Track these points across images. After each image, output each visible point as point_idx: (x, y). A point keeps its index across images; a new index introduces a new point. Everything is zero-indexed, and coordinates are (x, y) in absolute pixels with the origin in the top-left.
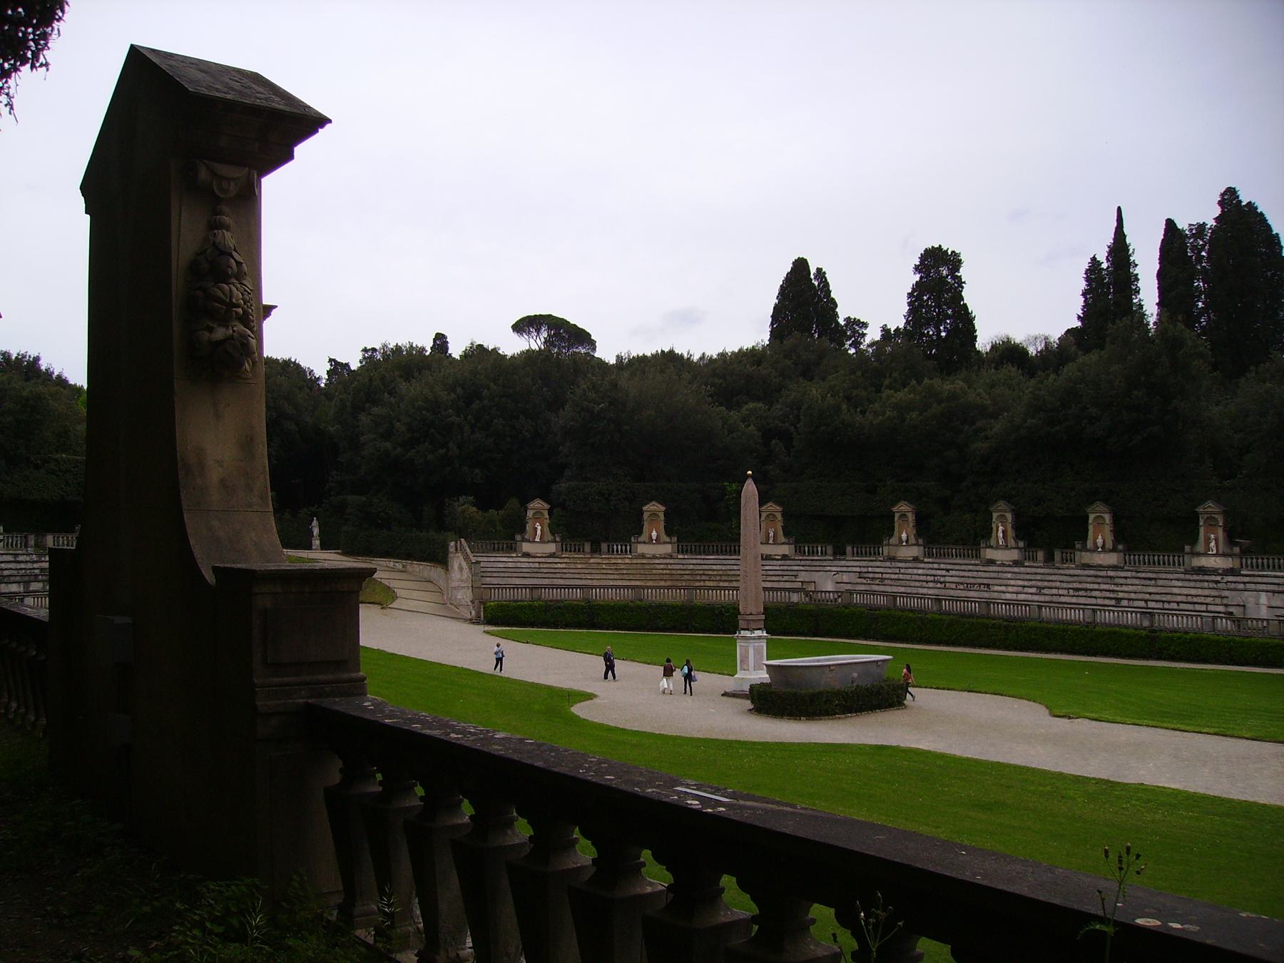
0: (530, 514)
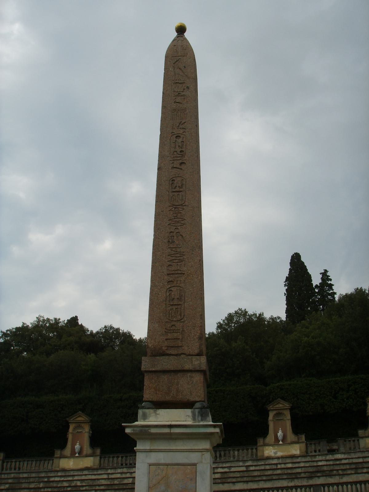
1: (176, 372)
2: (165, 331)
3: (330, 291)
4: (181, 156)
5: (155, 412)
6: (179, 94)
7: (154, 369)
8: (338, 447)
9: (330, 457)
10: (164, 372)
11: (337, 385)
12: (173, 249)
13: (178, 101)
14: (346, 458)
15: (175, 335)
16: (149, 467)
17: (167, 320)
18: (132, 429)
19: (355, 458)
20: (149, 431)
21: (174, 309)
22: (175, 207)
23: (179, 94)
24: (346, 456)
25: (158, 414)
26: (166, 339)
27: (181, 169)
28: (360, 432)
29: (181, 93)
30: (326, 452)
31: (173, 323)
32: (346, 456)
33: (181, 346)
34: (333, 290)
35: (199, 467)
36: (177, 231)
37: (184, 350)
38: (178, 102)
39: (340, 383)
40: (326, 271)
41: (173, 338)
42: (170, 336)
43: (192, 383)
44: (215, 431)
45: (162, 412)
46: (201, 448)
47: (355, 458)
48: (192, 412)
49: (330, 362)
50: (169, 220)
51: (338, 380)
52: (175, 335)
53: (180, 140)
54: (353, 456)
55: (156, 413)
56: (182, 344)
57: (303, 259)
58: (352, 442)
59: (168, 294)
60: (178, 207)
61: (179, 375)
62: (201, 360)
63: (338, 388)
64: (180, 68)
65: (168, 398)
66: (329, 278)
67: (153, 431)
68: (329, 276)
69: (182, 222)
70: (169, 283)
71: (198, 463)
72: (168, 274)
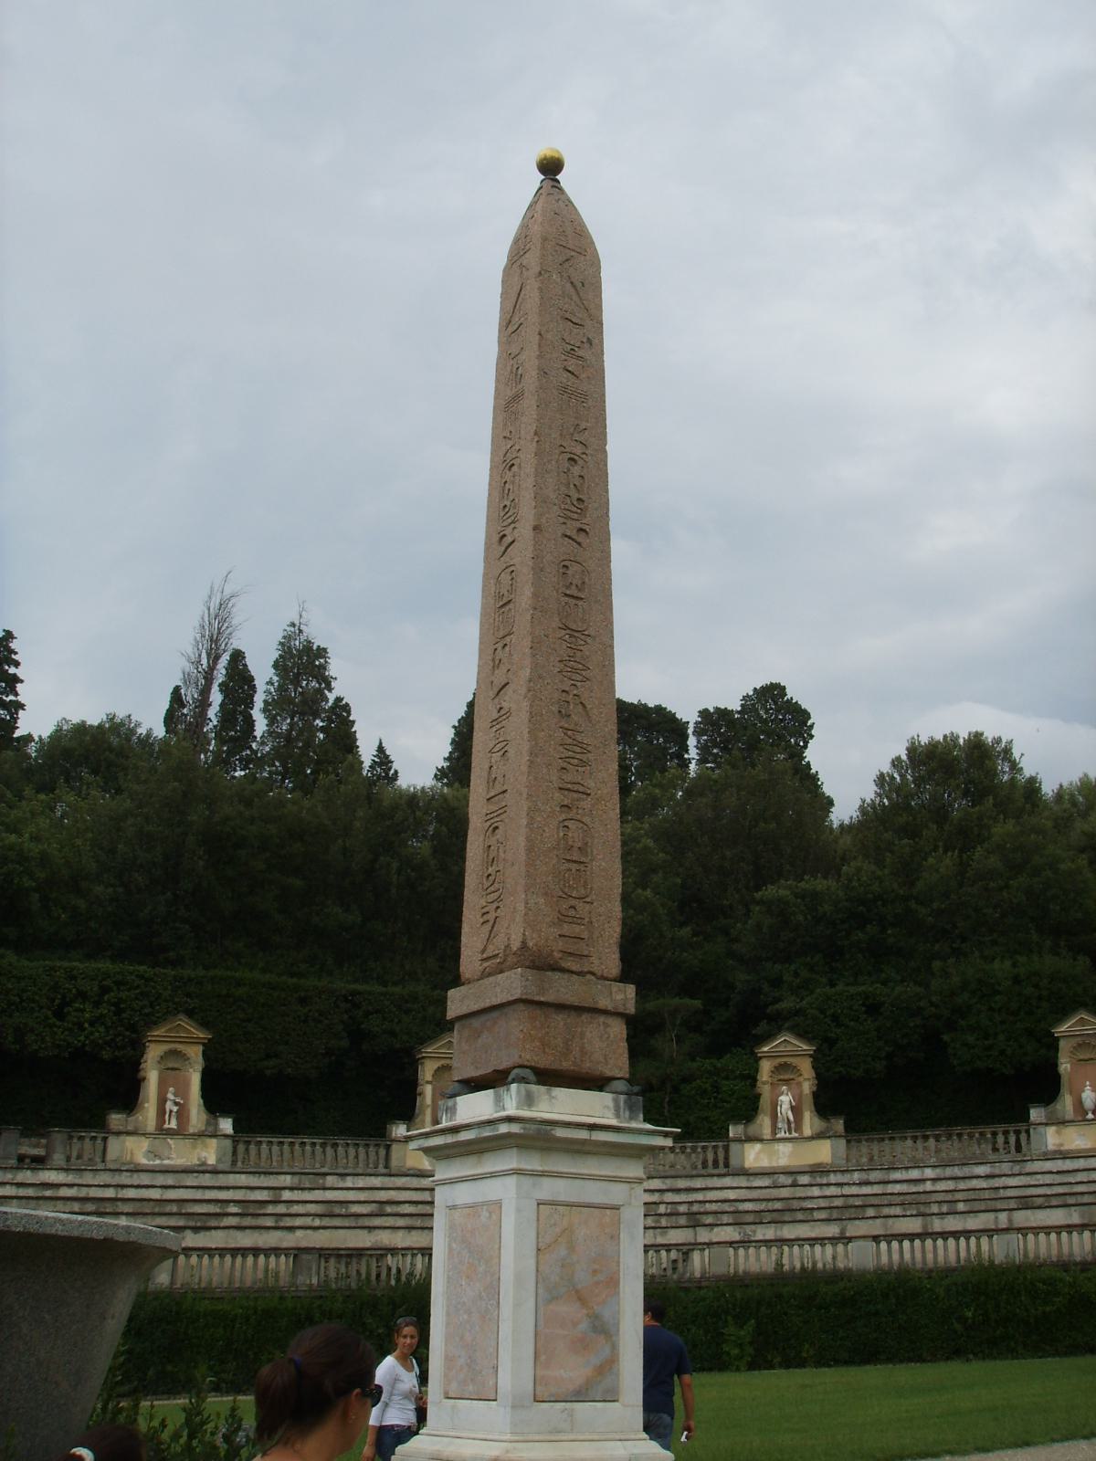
0: (766, 1067)
1: (579, 1009)
2: (558, 918)
3: (7, 697)
4: (579, 511)
5: (549, 1093)
6: (573, 352)
8: (47, 1152)
9: (26, 1176)
10: (561, 1007)
11: (73, 982)
12: (569, 732)
13: (570, 369)
14: (72, 1183)
15: (577, 929)
16: (536, 1207)
17: (561, 894)
18: (521, 1125)
19: (96, 1186)
20: (553, 1132)
21: (574, 870)
22: (568, 631)
23: (572, 349)
24: (70, 1178)
25: (553, 1097)
26: (560, 936)
27: (579, 544)
28: (115, 1119)
29: (576, 349)
30: (13, 1162)
31: (573, 902)
32: (70, 1178)
33: (586, 956)
34: (16, 694)
35: (626, 1214)
36: (575, 692)
37: (592, 965)
38: (570, 372)
39: (83, 979)
42: (566, 929)
43: (608, 1038)
44: (666, 1145)
45: (561, 1093)
46: (631, 1175)
47: (96, 1186)
49: (63, 916)
50: (560, 661)
51: (79, 969)
52: (577, 929)
53: (576, 470)
54: (88, 1178)
55: (550, 1095)
56: (590, 951)
58: (87, 1140)
59: (561, 834)
60: (576, 634)
61: (585, 1017)
62: (627, 994)
63: (74, 990)
64: (572, 283)
65: (566, 1065)
66: (13, 656)
67: (560, 1133)
68: (16, 653)
69: (584, 673)
70: (563, 809)
71: (623, 1205)
72: (560, 789)
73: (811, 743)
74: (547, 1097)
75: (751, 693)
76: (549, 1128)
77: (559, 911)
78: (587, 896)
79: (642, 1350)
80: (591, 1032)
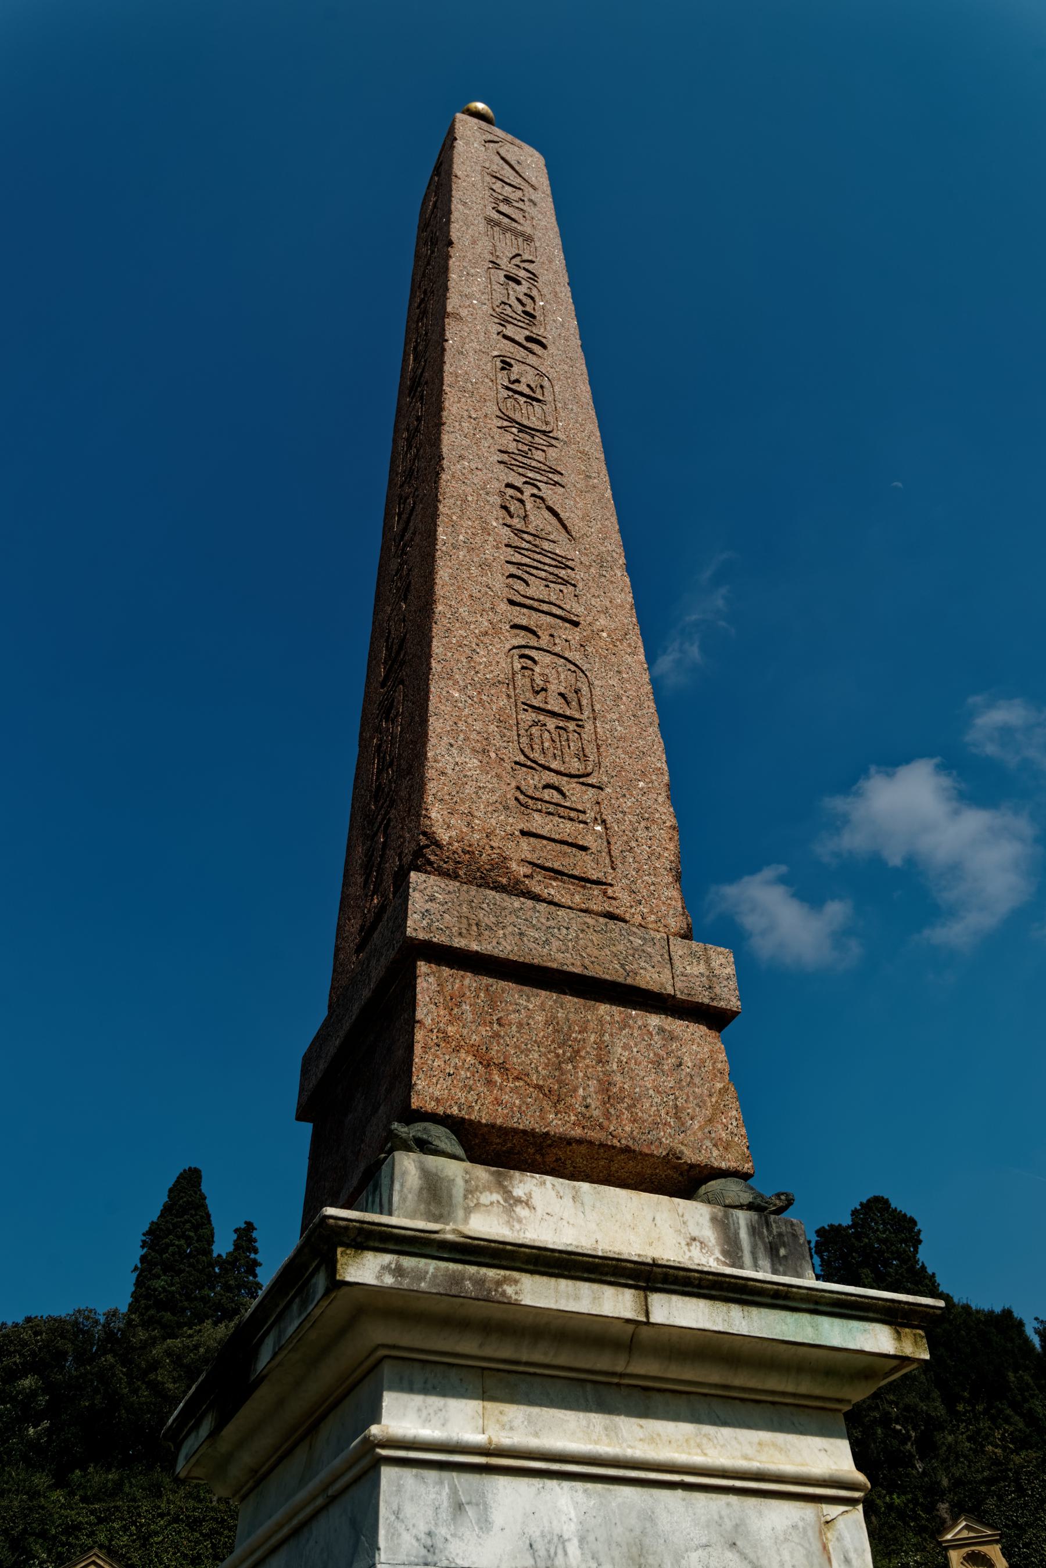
7: (475, 947)
17: (522, 758)
18: (387, 1258)
20: (509, 1290)
25: (518, 1201)
26: (523, 833)
34: (255, 1276)
40: (250, 1227)
41: (557, 837)
48: (714, 1219)
55: (507, 1193)
57: (205, 1188)
67: (536, 1293)
73: (921, 1247)
74: (496, 1197)
75: (859, 1207)
76: (491, 1273)
77: (518, 788)
78: (588, 775)
79: (726, 1432)
80: (625, 1047)
